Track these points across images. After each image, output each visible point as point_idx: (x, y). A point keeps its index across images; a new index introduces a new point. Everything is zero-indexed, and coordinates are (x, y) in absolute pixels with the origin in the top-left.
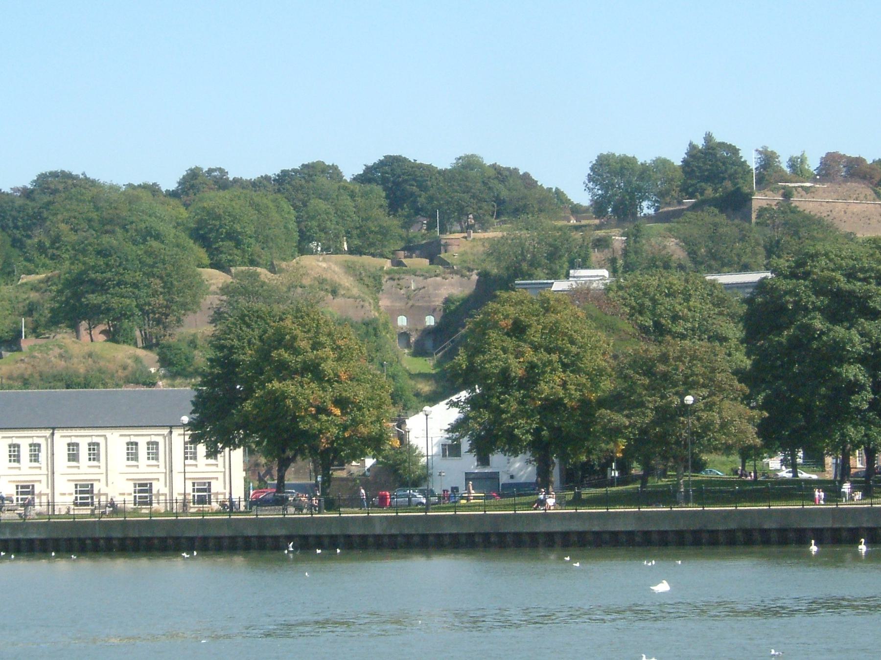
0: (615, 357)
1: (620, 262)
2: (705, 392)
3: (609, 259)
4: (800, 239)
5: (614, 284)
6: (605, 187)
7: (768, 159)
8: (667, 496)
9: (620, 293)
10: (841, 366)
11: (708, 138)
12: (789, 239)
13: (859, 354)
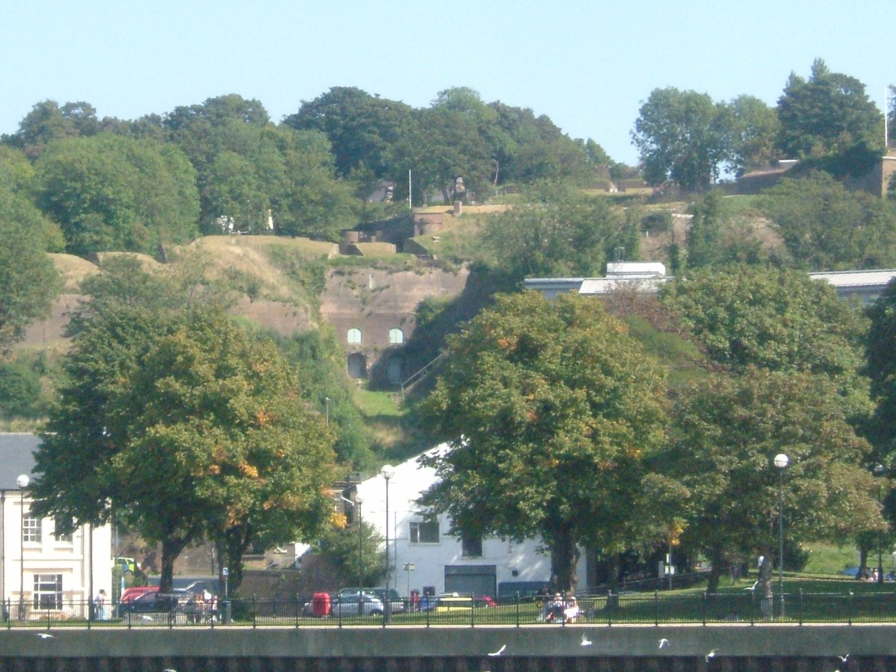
1: (683, 252)
2: (805, 449)
3: (665, 248)
6: (661, 139)
8: (747, 606)
9: (682, 298)
11: (818, 67)
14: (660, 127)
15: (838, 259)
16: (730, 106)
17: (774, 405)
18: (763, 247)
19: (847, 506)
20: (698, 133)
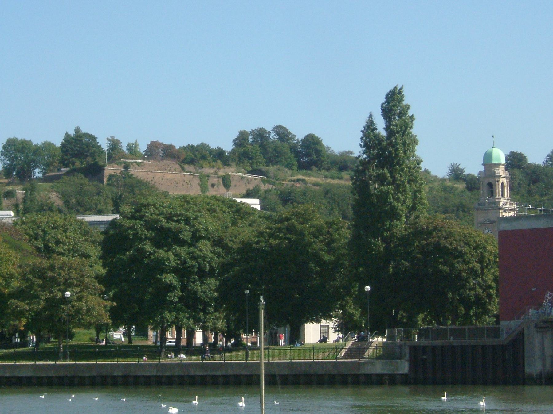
0: (20, 267)
1: (21, 206)
2: (77, 290)
3: (14, 205)
4: (134, 194)
5: (20, 221)
6: (12, 160)
7: (114, 144)
8: (53, 354)
9: (23, 226)
10: (162, 275)
11: (77, 130)
12: (127, 194)
13: (173, 267)
14: (11, 154)
15: (86, 211)
16: (41, 145)
17: (64, 271)
18: (55, 205)
19: (94, 313)
20: (27, 157)
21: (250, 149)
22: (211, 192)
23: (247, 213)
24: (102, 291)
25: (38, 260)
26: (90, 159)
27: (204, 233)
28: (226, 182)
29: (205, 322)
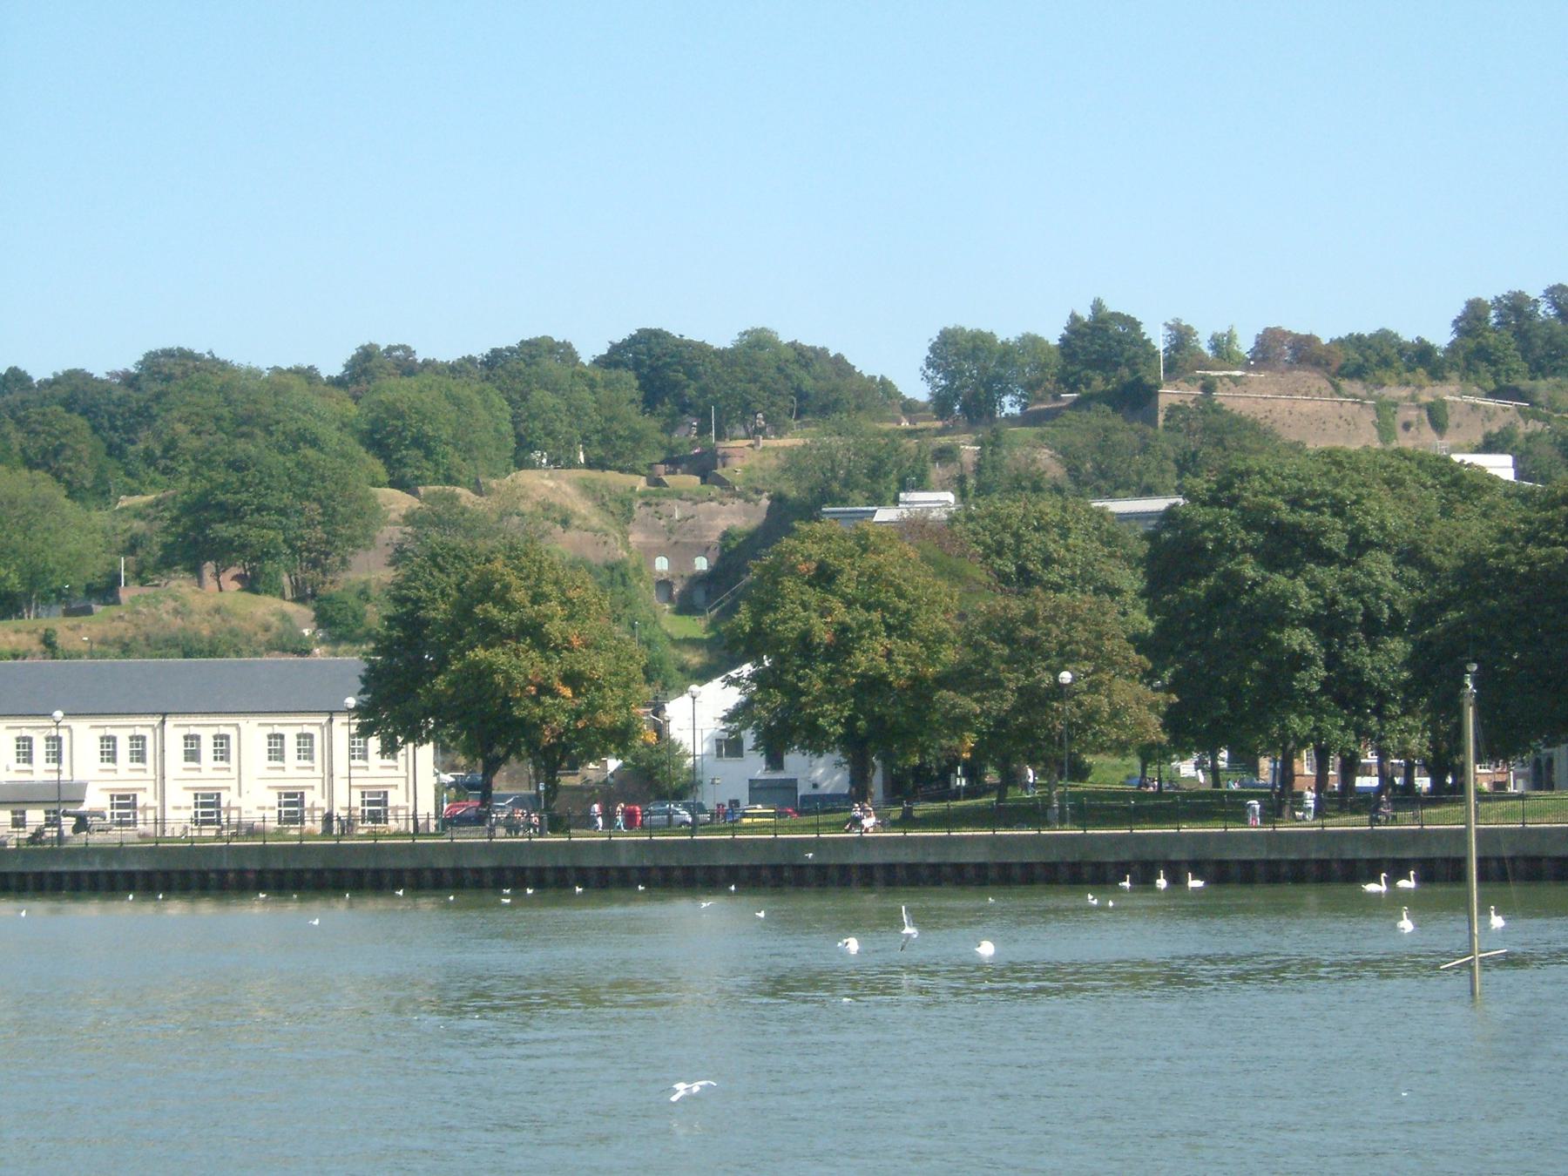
1: (972, 481)
2: (1088, 667)
5: (962, 513)
7: (1181, 337)
9: (970, 526)
10: (1282, 631)
11: (1097, 306)
14: (949, 365)
15: (1117, 488)
17: (1058, 626)
18: (1047, 476)
21: (1492, 341)
22: (1405, 441)
23: (1477, 488)
24: (1144, 670)
25: (1000, 601)
26: (1125, 372)
27: (1375, 535)
28: (1437, 418)
29: (1381, 738)
